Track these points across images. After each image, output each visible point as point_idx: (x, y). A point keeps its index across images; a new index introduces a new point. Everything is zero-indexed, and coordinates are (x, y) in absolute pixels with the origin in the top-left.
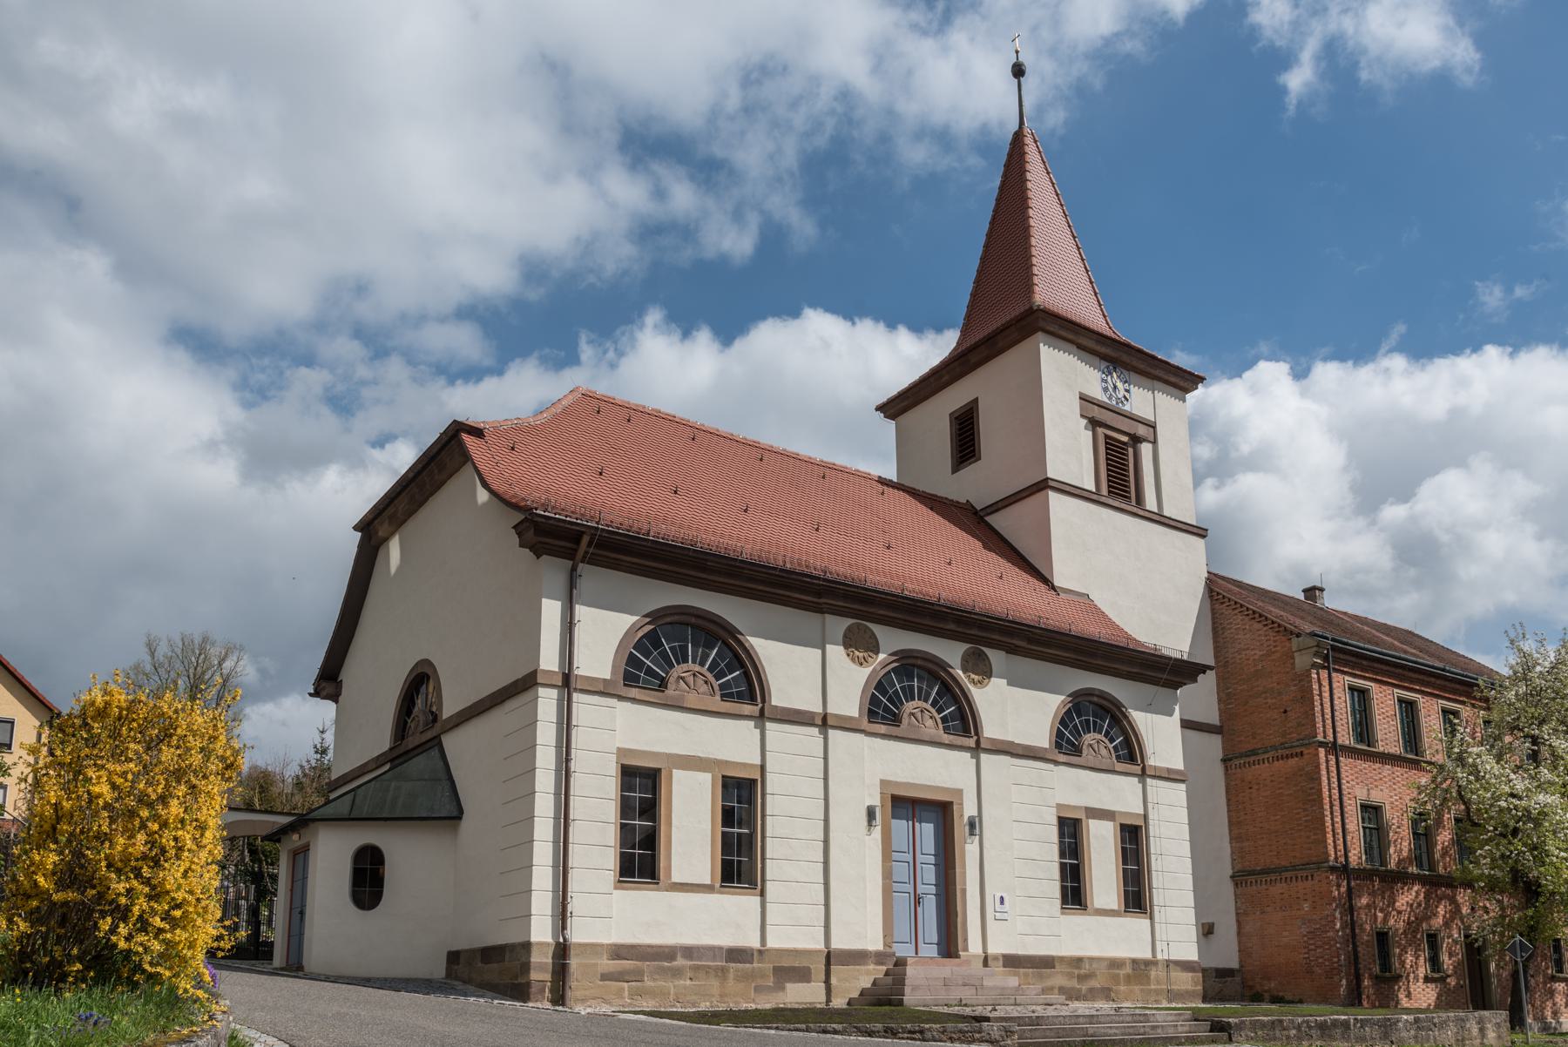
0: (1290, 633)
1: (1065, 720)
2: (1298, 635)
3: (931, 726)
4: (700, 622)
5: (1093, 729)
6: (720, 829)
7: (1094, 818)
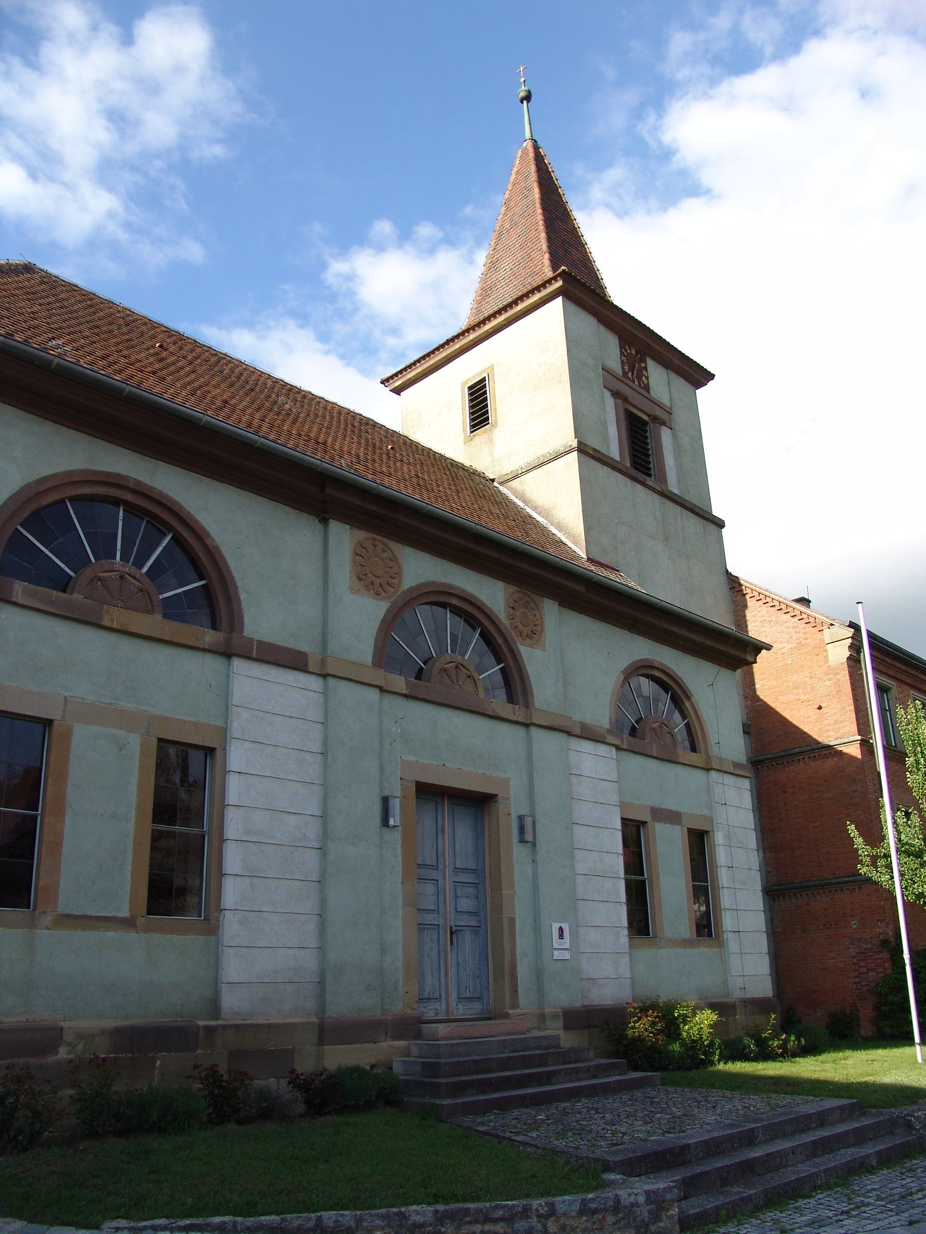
6: (691, 883)
7: (660, 821)
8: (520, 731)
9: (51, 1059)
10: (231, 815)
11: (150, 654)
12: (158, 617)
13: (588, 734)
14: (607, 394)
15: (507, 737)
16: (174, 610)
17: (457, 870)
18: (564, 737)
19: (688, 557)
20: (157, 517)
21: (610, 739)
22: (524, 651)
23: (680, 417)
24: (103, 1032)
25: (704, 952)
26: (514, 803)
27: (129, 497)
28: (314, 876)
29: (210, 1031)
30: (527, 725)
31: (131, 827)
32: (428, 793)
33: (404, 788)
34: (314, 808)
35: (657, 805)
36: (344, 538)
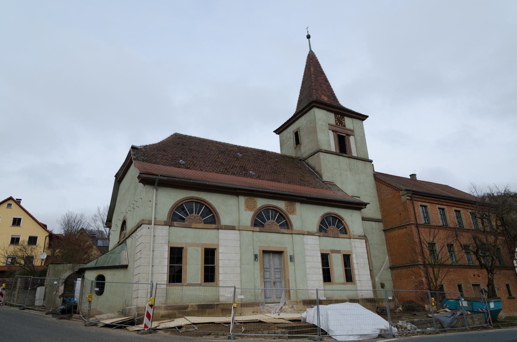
0: (398, 190)
1: (322, 222)
2: (402, 190)
3: (277, 226)
4: (197, 201)
5: (331, 226)
8: (291, 235)
9: (187, 310)
10: (220, 261)
11: (201, 231)
12: (203, 224)
13: (309, 234)
14: (331, 132)
15: (286, 238)
16: (206, 222)
17: (275, 269)
18: (302, 235)
19: (358, 174)
20: (201, 203)
21: (316, 234)
22: (290, 216)
23: (356, 132)
24: (196, 305)
25: (349, 286)
26: (289, 253)
27: (195, 200)
28: (239, 272)
29: (217, 305)
30: (292, 234)
31: (200, 266)
32: (265, 252)
33: (259, 252)
34: (239, 258)
35: (332, 249)
36: (242, 199)
